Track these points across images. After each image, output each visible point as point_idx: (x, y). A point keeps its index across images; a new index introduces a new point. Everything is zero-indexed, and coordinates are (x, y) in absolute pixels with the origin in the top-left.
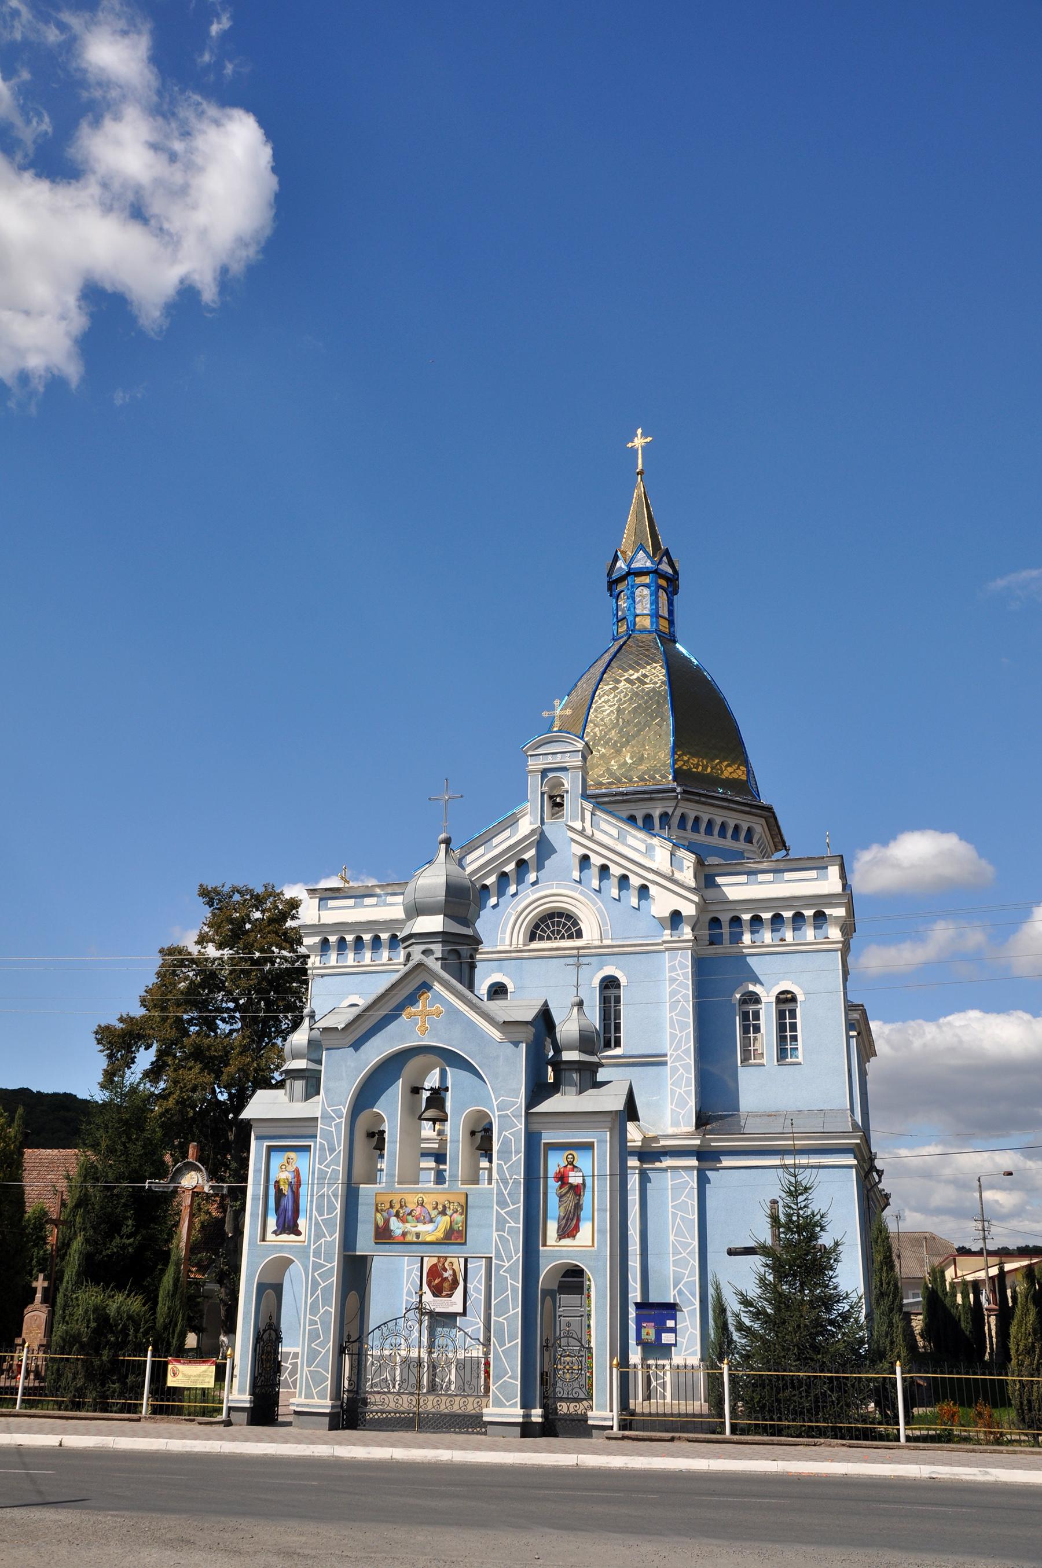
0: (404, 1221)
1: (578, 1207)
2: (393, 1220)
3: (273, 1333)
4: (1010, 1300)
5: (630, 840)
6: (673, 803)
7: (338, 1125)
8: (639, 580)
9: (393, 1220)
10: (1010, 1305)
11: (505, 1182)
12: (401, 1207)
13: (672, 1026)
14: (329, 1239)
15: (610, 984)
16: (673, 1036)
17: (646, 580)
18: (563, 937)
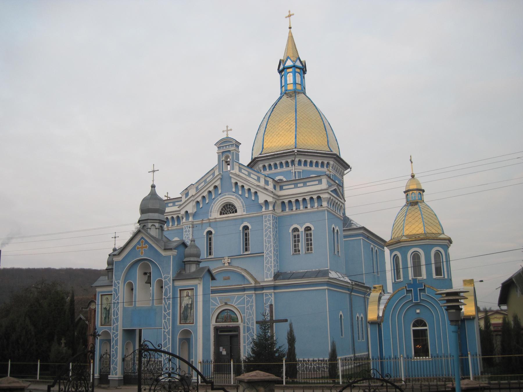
3: (108, 356)
5: (252, 176)
8: (289, 70)
11: (166, 304)
13: (266, 243)
15: (246, 228)
17: (291, 70)
18: (231, 213)
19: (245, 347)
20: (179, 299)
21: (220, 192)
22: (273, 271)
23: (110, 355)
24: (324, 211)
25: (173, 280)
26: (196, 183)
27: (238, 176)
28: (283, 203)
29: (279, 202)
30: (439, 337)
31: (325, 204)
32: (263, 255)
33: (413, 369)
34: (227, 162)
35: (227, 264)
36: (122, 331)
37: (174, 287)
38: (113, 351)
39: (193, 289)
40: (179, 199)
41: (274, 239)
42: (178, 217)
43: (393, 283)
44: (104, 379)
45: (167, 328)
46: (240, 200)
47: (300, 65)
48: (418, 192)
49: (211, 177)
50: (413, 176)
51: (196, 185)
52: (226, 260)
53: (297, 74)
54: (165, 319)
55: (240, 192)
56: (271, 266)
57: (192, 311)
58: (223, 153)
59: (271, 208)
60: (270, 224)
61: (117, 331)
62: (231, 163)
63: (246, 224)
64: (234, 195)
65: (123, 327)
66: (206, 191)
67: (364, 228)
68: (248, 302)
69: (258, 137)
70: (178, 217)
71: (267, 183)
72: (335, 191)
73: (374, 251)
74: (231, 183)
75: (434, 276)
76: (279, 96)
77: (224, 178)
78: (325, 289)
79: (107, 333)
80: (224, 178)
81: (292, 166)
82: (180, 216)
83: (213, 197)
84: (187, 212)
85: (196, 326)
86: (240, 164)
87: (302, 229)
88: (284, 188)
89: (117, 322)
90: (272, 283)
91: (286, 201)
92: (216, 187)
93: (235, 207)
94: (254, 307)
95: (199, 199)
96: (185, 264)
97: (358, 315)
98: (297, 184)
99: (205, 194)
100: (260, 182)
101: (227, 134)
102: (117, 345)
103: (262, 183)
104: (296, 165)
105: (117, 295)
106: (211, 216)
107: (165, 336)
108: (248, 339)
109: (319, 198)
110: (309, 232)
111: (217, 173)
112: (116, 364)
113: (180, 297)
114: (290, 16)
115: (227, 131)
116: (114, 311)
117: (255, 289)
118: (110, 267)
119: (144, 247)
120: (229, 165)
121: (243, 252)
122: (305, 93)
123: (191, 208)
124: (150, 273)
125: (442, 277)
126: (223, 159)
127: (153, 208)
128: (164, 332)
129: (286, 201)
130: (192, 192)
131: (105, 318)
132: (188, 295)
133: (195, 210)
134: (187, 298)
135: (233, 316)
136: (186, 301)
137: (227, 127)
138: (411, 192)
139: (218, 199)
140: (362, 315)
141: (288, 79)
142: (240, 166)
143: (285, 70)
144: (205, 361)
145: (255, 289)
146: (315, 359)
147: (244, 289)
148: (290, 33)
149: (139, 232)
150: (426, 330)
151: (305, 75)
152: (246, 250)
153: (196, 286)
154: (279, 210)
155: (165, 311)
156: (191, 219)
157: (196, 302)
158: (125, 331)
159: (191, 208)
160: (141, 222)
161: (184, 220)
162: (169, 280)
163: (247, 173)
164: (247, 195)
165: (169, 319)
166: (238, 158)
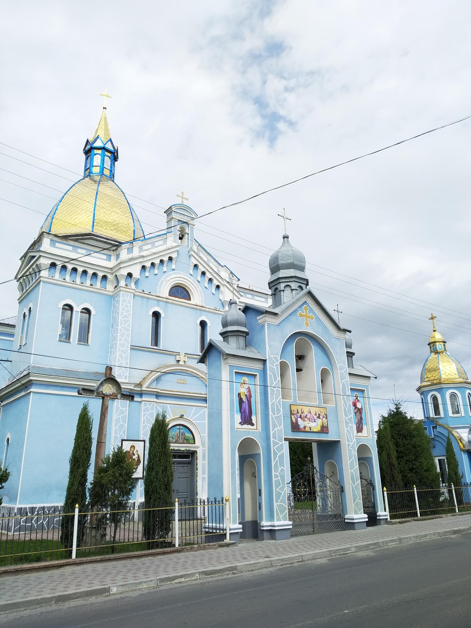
0: (304, 421)
1: (361, 418)
2: (299, 419)
4: (447, 469)
7: (276, 365)
8: (96, 151)
9: (299, 419)
10: (438, 470)
11: (346, 405)
12: (302, 413)
14: (279, 428)
17: (99, 152)
53: (106, 158)
139: (171, 275)
151: (116, 163)
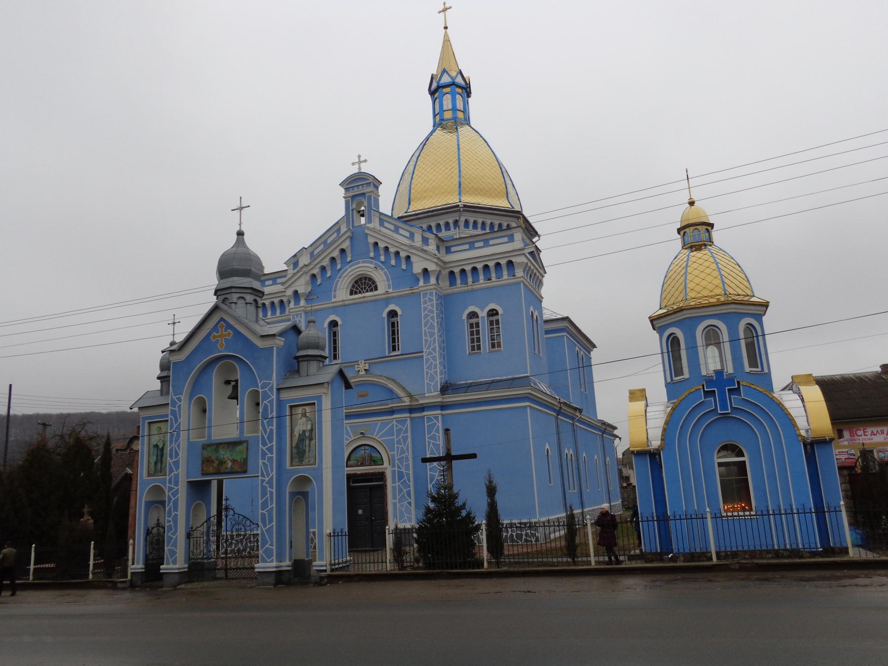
5: (401, 231)
6: (457, 214)
11: (266, 432)
15: (393, 314)
16: (426, 341)
18: (367, 291)
19: (395, 504)
20: (288, 418)
21: (349, 259)
22: (439, 380)
23: (164, 528)
24: (519, 283)
25: (279, 390)
26: (311, 246)
27: (378, 232)
28: (452, 273)
29: (445, 272)
30: (772, 476)
31: (519, 273)
32: (422, 357)
33: (727, 534)
34: (359, 212)
35: (364, 372)
36: (185, 483)
37: (280, 403)
38: (169, 521)
39: (314, 404)
40: (281, 274)
41: (439, 331)
42: (282, 302)
43: (667, 385)
44: (153, 575)
45: (268, 475)
46: (382, 269)
47: (462, 82)
48: (704, 227)
49: (335, 235)
50: (692, 203)
51: (311, 249)
52: (362, 366)
53: (458, 96)
54: (263, 458)
55: (382, 258)
56: (436, 373)
57: (313, 442)
58: (353, 197)
59: (433, 280)
60: (432, 305)
61: (176, 484)
62: (366, 213)
63: (392, 307)
64: (371, 263)
65: (188, 478)
66: (325, 259)
67: (567, 319)
68: (399, 431)
69: (400, 189)
70: (282, 302)
71: (425, 241)
72: (531, 253)
73: (580, 356)
74: (368, 243)
75: (747, 369)
76: (431, 129)
77: (357, 236)
78: (526, 407)
79: (158, 490)
80: (357, 236)
81: (455, 228)
82: (285, 299)
83: (339, 267)
84: (296, 292)
85: (320, 468)
86: (381, 213)
87: (483, 314)
88: (453, 249)
89: (177, 468)
90: (439, 400)
91: (457, 270)
92: (343, 251)
93: (374, 282)
94: (409, 440)
95: (316, 271)
96: (298, 362)
97: (566, 451)
98: (473, 243)
99: (326, 262)
100: (413, 241)
101: (360, 168)
102: (176, 509)
103: (418, 241)
104: (462, 227)
105: (176, 421)
106: (335, 297)
107: (264, 489)
108: (401, 491)
109: (510, 263)
110: (494, 318)
111: (344, 229)
112: (175, 545)
113: (291, 415)
114: (445, 10)
115: (360, 162)
116: (171, 449)
117: (411, 410)
118: (165, 374)
119: (225, 335)
120: (363, 215)
121: (389, 352)
122: (469, 124)
123: (302, 286)
124: (237, 381)
125: (759, 369)
126: (354, 206)
127: (238, 271)
128: (263, 481)
129: (457, 270)
130: (304, 260)
131: (156, 463)
132: (304, 415)
133: (309, 289)
134: (304, 419)
135: (375, 455)
136: (302, 425)
137: (359, 156)
138: (692, 228)
140: (571, 452)
141: (445, 103)
142: (382, 217)
143: (440, 90)
144: (338, 530)
145: (411, 410)
146: (514, 521)
147: (392, 412)
148: (446, 35)
149: (215, 308)
150: (744, 462)
152: (394, 349)
153: (319, 398)
154: (445, 283)
155: (264, 444)
156: (302, 303)
157: (320, 422)
158: (192, 484)
159: (302, 286)
160: (219, 293)
161: (292, 305)
162: (271, 390)
163: (392, 227)
164: (393, 262)
165: (271, 459)
166: (377, 205)
